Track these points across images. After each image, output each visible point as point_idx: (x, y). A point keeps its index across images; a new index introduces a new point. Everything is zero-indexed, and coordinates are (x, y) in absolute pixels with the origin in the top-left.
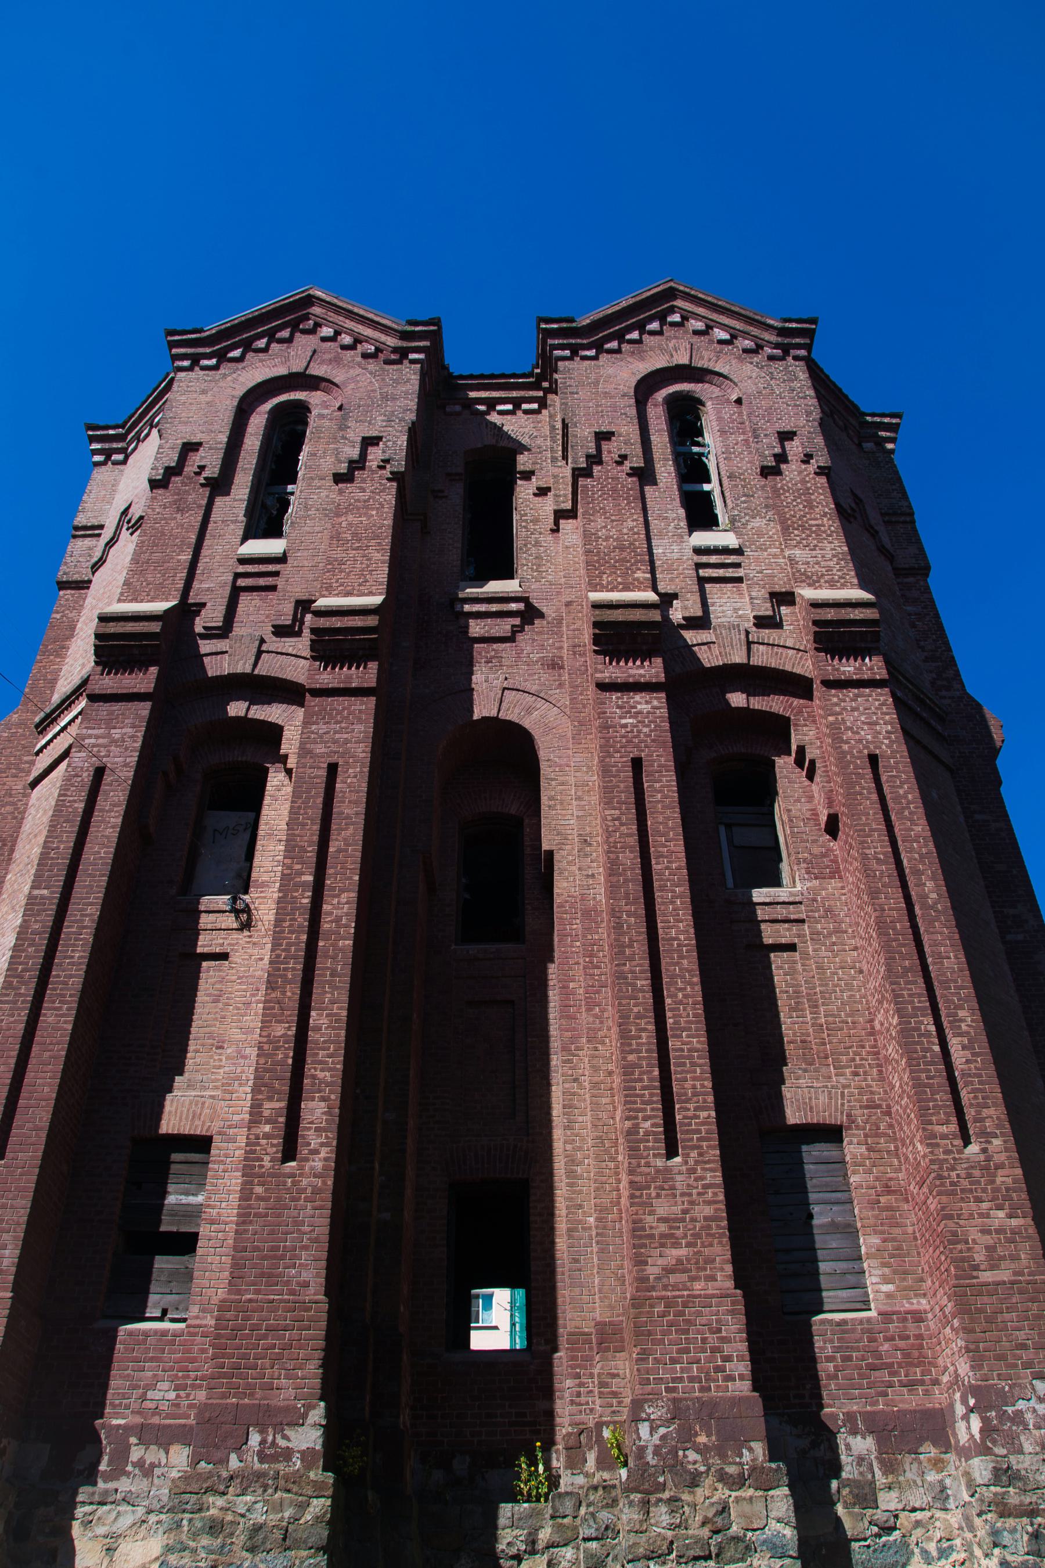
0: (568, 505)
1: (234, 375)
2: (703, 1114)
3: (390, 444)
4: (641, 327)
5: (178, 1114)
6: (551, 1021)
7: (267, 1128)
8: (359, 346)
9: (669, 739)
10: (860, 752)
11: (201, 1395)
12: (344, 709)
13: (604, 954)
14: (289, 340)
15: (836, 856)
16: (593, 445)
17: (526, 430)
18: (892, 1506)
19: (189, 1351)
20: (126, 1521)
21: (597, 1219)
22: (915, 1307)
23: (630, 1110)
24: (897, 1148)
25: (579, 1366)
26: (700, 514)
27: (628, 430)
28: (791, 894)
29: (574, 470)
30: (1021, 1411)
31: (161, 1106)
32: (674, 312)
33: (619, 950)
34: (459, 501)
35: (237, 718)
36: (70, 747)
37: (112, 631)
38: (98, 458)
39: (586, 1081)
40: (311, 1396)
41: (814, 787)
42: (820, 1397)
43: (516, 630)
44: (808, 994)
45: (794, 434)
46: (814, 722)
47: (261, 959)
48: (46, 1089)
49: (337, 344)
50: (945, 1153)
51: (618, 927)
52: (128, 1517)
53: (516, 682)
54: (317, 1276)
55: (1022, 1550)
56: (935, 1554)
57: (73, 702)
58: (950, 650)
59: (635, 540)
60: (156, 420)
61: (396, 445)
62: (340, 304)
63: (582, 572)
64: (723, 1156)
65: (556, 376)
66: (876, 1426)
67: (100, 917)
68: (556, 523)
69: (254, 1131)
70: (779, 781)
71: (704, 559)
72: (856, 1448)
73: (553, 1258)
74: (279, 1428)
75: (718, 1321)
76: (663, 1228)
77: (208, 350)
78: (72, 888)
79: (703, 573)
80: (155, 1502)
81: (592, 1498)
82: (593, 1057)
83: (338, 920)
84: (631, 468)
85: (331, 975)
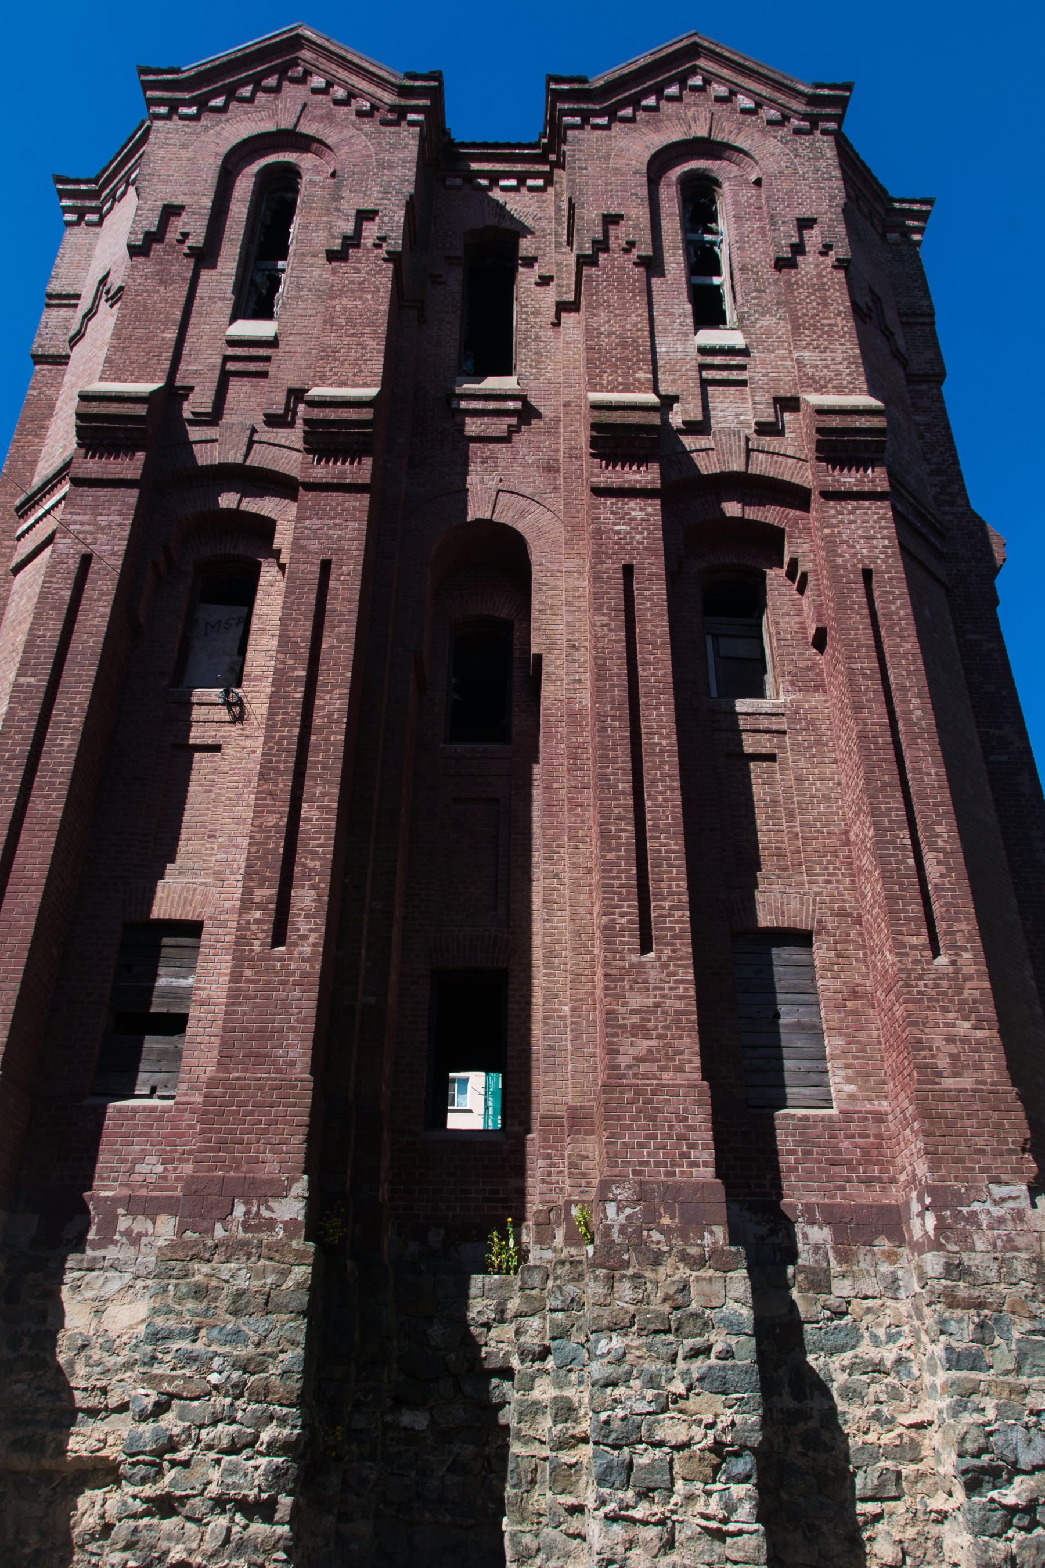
0: (570, 297)
1: (218, 129)
2: (678, 913)
3: (386, 219)
4: (658, 91)
5: (169, 900)
6: (535, 820)
7: (258, 914)
8: (353, 102)
9: (662, 547)
10: (854, 566)
11: (188, 1169)
12: (338, 505)
13: (588, 757)
14: (276, 90)
15: (821, 670)
16: (599, 229)
17: (530, 210)
18: (845, 1293)
19: (177, 1127)
20: (114, 1286)
21: (573, 1009)
22: (876, 1108)
23: (608, 906)
24: (865, 956)
25: (550, 1147)
26: (708, 310)
27: (638, 213)
28: (774, 706)
29: (579, 257)
30: (976, 1212)
31: (152, 892)
32: (695, 74)
33: (602, 753)
34: (457, 286)
35: (229, 510)
36: (54, 533)
37: (95, 411)
38: (70, 217)
39: (566, 878)
40: (295, 1169)
41: (804, 600)
42: (780, 1187)
43: (513, 430)
44: (785, 804)
45: (814, 221)
46: (809, 534)
47: (254, 752)
48: (36, 875)
49: (329, 98)
50: (913, 962)
51: (603, 730)
52: (116, 1282)
53: (511, 484)
54: (304, 1055)
55: (967, 1338)
56: (883, 1338)
57: (56, 486)
58: (957, 463)
59: (638, 337)
60: (133, 176)
61: (393, 220)
62: (332, 48)
63: (583, 370)
64: (695, 953)
65: (564, 148)
66: (833, 1217)
67: (90, 706)
68: (558, 316)
69: (245, 916)
70: (769, 593)
71: (709, 360)
72: (813, 1237)
73: (528, 1044)
74: (263, 1199)
75: (685, 1110)
76: (635, 1019)
77: (187, 96)
78: (60, 676)
79: (706, 374)
80: (142, 1268)
81: (559, 1272)
82: (573, 854)
83: (330, 715)
84: (639, 257)
85: (323, 769)
